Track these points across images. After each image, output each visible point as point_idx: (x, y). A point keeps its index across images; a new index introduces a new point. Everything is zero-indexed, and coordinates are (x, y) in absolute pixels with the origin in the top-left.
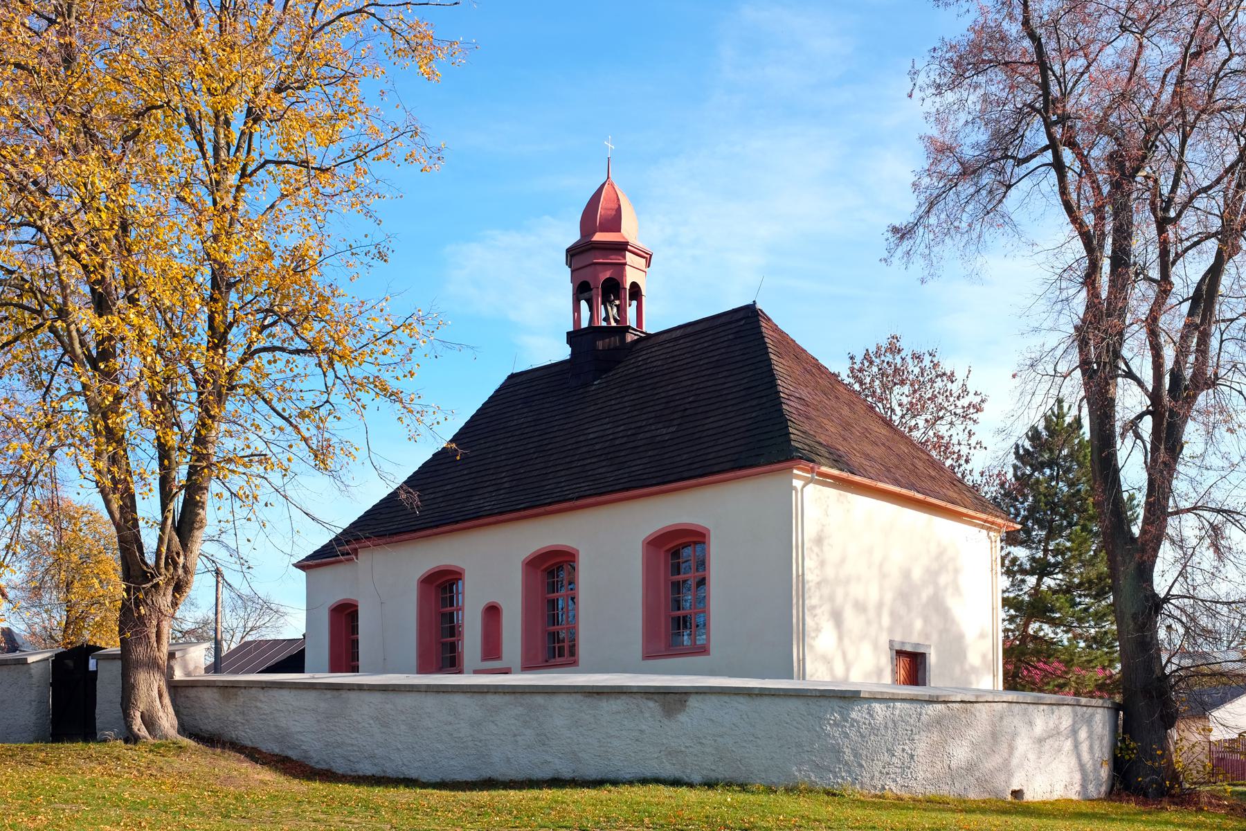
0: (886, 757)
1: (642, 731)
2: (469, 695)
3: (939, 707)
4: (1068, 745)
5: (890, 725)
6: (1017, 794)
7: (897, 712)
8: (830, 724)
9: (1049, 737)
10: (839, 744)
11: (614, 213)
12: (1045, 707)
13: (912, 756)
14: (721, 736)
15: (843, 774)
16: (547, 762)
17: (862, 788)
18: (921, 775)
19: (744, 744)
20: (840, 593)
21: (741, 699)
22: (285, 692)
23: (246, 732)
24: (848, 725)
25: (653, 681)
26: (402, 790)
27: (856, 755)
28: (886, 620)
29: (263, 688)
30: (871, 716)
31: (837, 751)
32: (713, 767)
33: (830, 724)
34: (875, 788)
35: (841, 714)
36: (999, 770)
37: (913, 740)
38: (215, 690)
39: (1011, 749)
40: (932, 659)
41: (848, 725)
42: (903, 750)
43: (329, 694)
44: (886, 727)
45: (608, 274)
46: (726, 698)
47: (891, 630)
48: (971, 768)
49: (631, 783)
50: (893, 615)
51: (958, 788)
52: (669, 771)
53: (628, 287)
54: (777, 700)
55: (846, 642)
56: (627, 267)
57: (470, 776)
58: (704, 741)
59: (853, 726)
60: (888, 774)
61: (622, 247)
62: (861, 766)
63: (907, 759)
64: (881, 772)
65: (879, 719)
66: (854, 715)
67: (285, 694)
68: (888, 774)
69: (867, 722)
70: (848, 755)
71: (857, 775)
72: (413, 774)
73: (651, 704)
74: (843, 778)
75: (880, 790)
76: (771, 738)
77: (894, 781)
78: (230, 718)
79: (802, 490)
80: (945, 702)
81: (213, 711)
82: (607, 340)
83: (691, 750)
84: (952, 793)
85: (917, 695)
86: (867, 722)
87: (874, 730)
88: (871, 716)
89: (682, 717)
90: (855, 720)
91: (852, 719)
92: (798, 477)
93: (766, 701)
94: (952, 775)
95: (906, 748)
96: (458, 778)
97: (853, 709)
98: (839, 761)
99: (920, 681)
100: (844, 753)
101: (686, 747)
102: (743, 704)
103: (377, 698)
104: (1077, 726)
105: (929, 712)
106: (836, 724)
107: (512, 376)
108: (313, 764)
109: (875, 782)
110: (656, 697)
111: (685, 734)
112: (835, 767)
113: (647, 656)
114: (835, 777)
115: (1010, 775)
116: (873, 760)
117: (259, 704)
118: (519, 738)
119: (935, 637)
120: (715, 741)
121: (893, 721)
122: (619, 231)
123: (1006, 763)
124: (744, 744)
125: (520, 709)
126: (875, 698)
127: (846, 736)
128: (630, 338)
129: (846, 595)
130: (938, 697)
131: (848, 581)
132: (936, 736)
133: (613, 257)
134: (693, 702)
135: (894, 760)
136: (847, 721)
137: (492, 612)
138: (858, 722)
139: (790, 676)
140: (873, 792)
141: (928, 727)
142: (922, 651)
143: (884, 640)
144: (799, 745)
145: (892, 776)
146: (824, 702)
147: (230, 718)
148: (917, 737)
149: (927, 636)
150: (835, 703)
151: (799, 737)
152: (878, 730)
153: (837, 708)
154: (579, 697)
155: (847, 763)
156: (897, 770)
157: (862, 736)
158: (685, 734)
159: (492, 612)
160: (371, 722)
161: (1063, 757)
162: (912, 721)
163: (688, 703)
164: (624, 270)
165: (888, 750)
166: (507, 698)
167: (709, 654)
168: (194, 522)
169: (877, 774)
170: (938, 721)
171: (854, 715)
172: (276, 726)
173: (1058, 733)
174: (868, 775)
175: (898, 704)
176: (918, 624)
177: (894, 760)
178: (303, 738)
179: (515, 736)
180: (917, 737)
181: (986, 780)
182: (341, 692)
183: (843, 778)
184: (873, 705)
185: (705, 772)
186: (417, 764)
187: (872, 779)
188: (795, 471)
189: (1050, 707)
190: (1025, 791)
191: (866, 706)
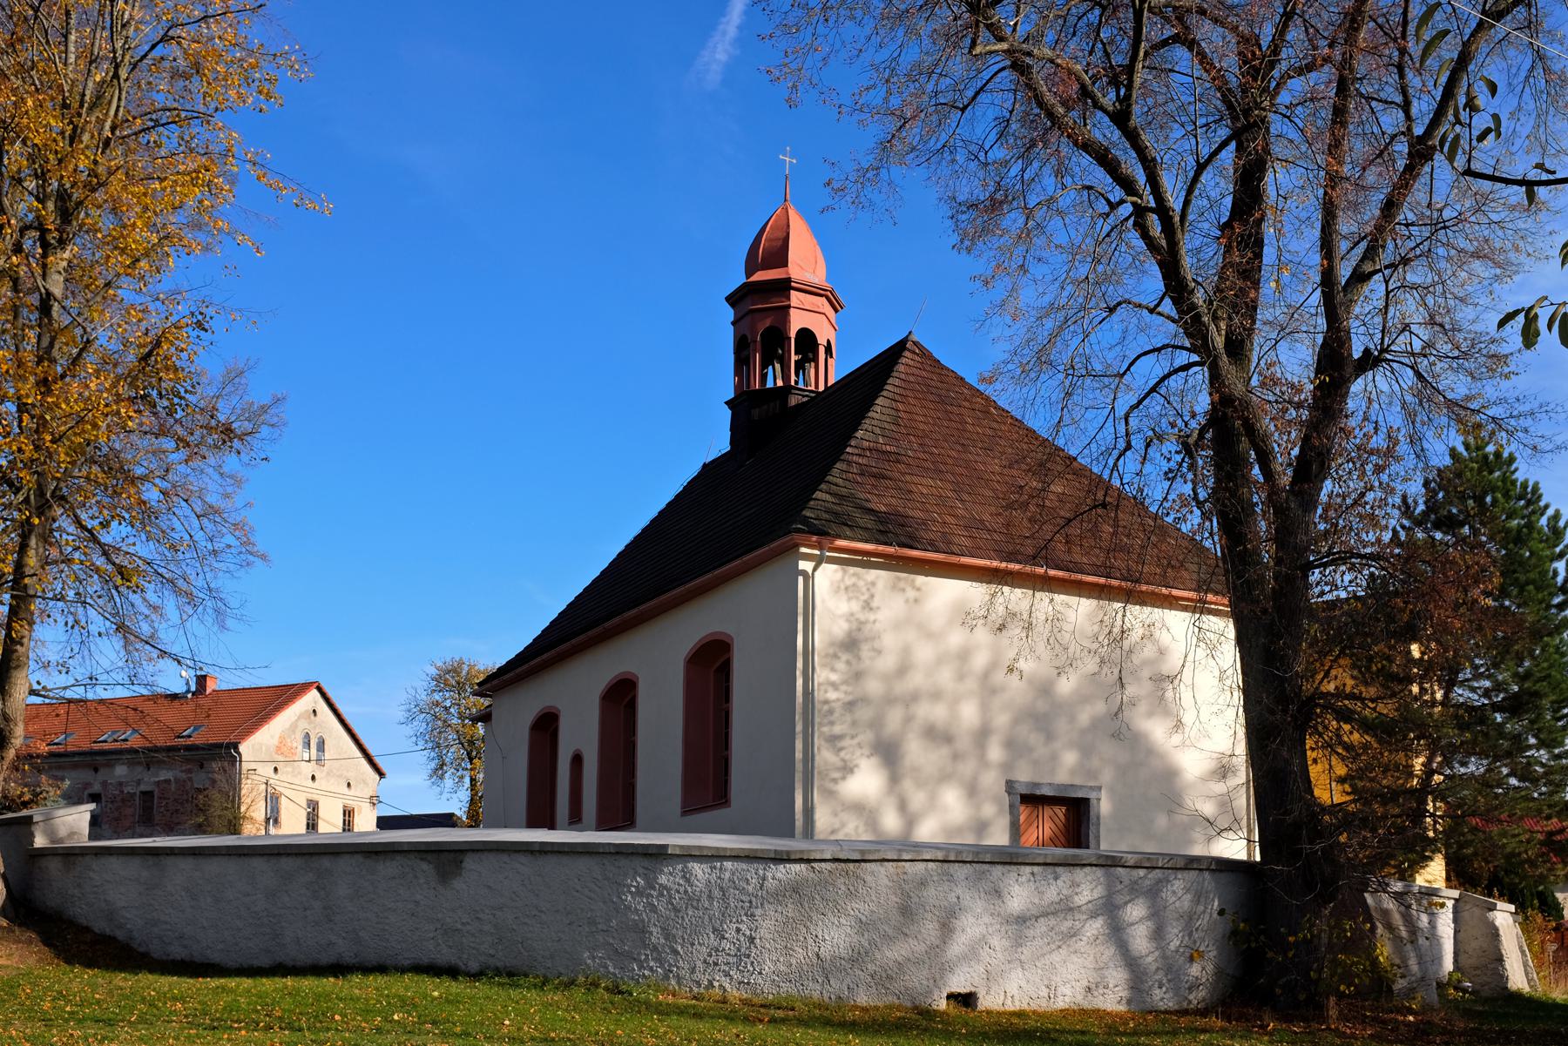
0: (713, 940)
1: (417, 903)
2: (265, 858)
3: (796, 867)
4: (1096, 926)
5: (717, 893)
6: (966, 1000)
7: (727, 875)
8: (631, 892)
9: (1045, 914)
10: (643, 921)
11: (780, 243)
12: (1036, 869)
13: (752, 940)
14: (501, 909)
15: (652, 964)
16: (330, 944)
17: (679, 983)
18: (768, 967)
19: (526, 920)
20: (894, 718)
21: (522, 858)
22: (113, 859)
23: (82, 909)
24: (655, 893)
25: (638, 838)
26: (356, 979)
27: (668, 936)
28: (995, 753)
29: (96, 854)
30: (688, 880)
31: (641, 930)
32: (492, 952)
33: (631, 892)
34: (699, 984)
35: (645, 877)
36: (918, 963)
37: (753, 915)
38: (59, 858)
39: (946, 930)
40: (1104, 806)
41: (655, 893)
42: (738, 930)
43: (151, 860)
44: (710, 897)
45: (767, 323)
46: (505, 857)
47: (1007, 766)
48: (857, 958)
49: (403, 970)
50: (1010, 744)
51: (837, 987)
52: (445, 956)
53: (793, 334)
54: (565, 859)
55: (907, 785)
56: (792, 311)
57: (265, 961)
58: (481, 916)
59: (663, 895)
60: (716, 964)
61: (784, 286)
62: (676, 952)
63: (745, 944)
64: (705, 961)
65: (700, 885)
66: (663, 879)
67: (114, 862)
68: (716, 964)
69: (682, 889)
70: (656, 936)
71: (670, 965)
72: (216, 957)
73: (425, 866)
74: (651, 969)
75: (707, 988)
76: (557, 911)
77: (727, 974)
78: (69, 892)
79: (813, 574)
80: (809, 861)
81: (57, 887)
82: (765, 407)
83: (469, 927)
84: (825, 995)
85: (756, 850)
86: (682, 889)
87: (692, 900)
88: (688, 880)
89: (458, 884)
90: (665, 887)
91: (661, 885)
92: (807, 557)
93: (551, 861)
94: (825, 968)
95: (743, 927)
96: (256, 963)
97: (662, 872)
98: (645, 946)
99: (1083, 845)
100: (651, 933)
101: (463, 924)
102: (523, 864)
103: (186, 864)
104: (1119, 899)
105: (779, 875)
106: (640, 893)
107: (706, 467)
108: (135, 946)
109: (698, 976)
110: (429, 857)
111: (461, 907)
112: (639, 954)
113: (685, 813)
114: (641, 967)
115: (946, 969)
116: (693, 944)
117: (91, 874)
118: (308, 912)
119: (1107, 776)
120: (494, 915)
121: (722, 889)
122: (786, 265)
123: (936, 950)
124: (526, 920)
125: (311, 875)
126: (691, 856)
127: (654, 909)
128: (793, 400)
129: (908, 720)
130: (788, 853)
131: (914, 698)
132: (791, 910)
133: (773, 300)
134: (470, 862)
135: (726, 945)
136: (654, 889)
137: (577, 760)
138: (669, 890)
139: (789, 833)
140: (696, 990)
141: (778, 896)
142: (1080, 795)
143: (992, 781)
144: (592, 922)
145: (723, 967)
146: (623, 862)
147: (69, 892)
148: (758, 912)
149: (1092, 774)
150: (639, 863)
151: (592, 910)
152: (699, 900)
153: (641, 871)
154: (359, 858)
155: (655, 948)
156: (731, 960)
157: (676, 910)
158: (461, 907)
159: (577, 760)
160: (183, 893)
161: (1082, 945)
162: (750, 888)
163: (464, 865)
164: (788, 314)
165: (715, 930)
166: (299, 861)
167: (730, 806)
168: (10, 661)
169: (699, 964)
170: (795, 889)
171: (663, 879)
172: (105, 900)
173: (537, 895)
174: (687, 966)
175: (728, 865)
176: (1070, 758)
177: (726, 945)
178: (128, 915)
179: (305, 909)
180: (758, 912)
181: (889, 977)
182: (162, 858)
183: (651, 969)
184: (690, 865)
185: (482, 959)
186: (220, 946)
187: (693, 970)
188: (803, 550)
189: (1050, 869)
190: (980, 996)
191: (680, 867)
